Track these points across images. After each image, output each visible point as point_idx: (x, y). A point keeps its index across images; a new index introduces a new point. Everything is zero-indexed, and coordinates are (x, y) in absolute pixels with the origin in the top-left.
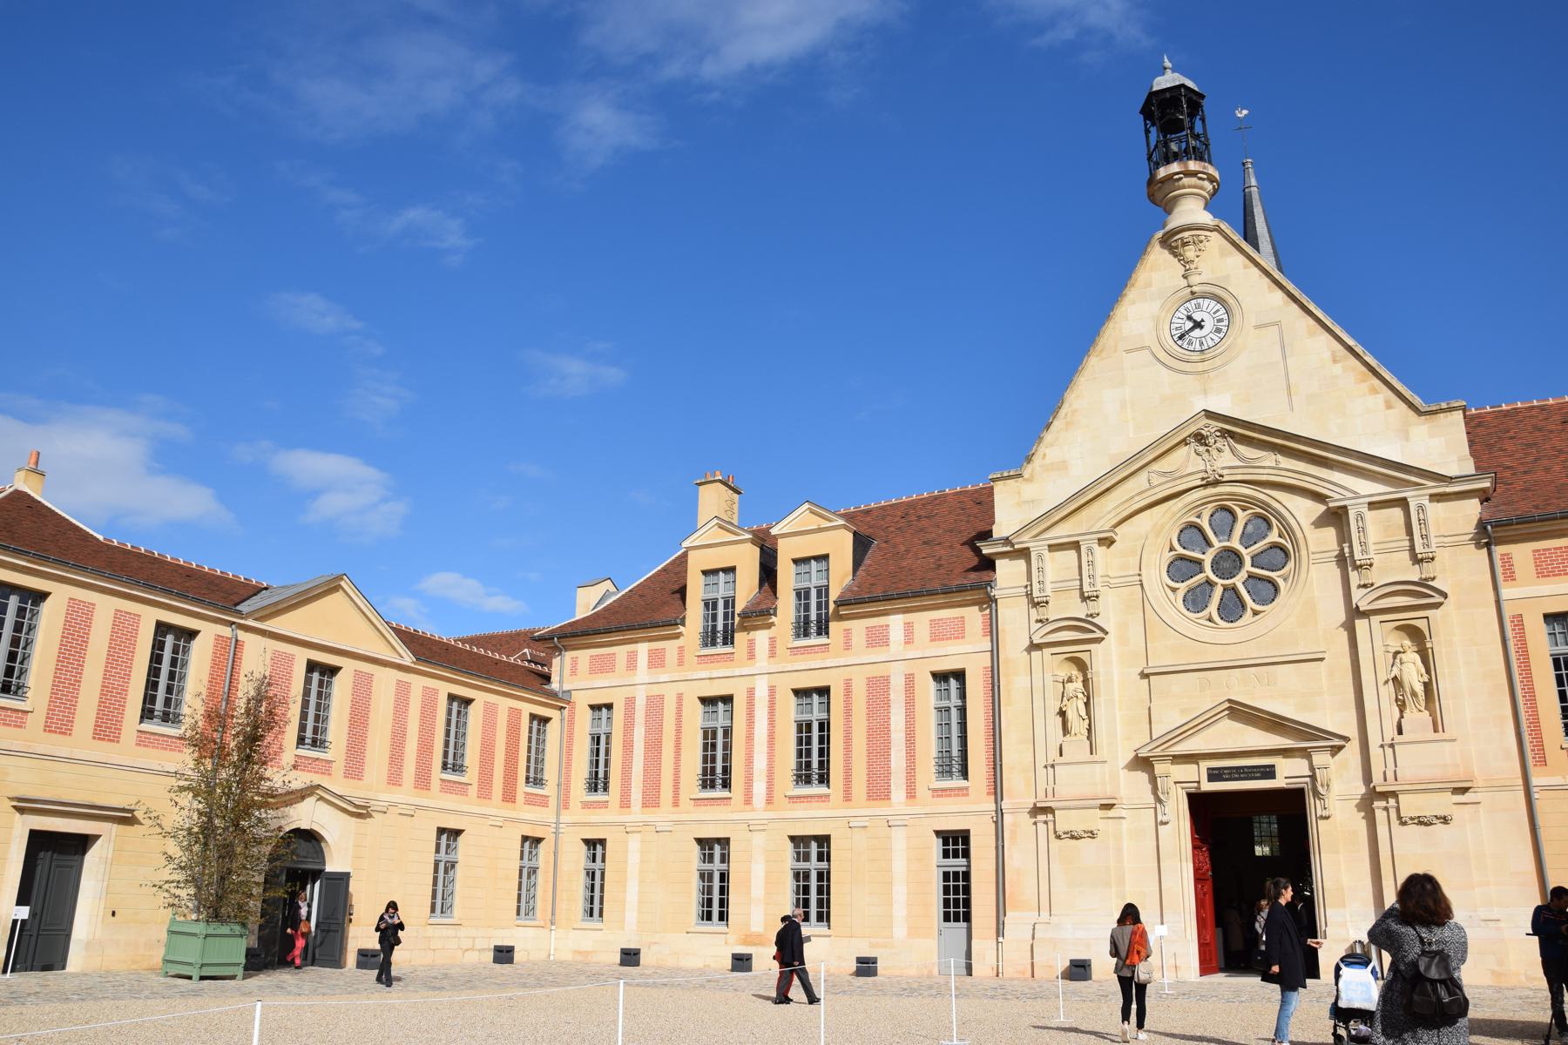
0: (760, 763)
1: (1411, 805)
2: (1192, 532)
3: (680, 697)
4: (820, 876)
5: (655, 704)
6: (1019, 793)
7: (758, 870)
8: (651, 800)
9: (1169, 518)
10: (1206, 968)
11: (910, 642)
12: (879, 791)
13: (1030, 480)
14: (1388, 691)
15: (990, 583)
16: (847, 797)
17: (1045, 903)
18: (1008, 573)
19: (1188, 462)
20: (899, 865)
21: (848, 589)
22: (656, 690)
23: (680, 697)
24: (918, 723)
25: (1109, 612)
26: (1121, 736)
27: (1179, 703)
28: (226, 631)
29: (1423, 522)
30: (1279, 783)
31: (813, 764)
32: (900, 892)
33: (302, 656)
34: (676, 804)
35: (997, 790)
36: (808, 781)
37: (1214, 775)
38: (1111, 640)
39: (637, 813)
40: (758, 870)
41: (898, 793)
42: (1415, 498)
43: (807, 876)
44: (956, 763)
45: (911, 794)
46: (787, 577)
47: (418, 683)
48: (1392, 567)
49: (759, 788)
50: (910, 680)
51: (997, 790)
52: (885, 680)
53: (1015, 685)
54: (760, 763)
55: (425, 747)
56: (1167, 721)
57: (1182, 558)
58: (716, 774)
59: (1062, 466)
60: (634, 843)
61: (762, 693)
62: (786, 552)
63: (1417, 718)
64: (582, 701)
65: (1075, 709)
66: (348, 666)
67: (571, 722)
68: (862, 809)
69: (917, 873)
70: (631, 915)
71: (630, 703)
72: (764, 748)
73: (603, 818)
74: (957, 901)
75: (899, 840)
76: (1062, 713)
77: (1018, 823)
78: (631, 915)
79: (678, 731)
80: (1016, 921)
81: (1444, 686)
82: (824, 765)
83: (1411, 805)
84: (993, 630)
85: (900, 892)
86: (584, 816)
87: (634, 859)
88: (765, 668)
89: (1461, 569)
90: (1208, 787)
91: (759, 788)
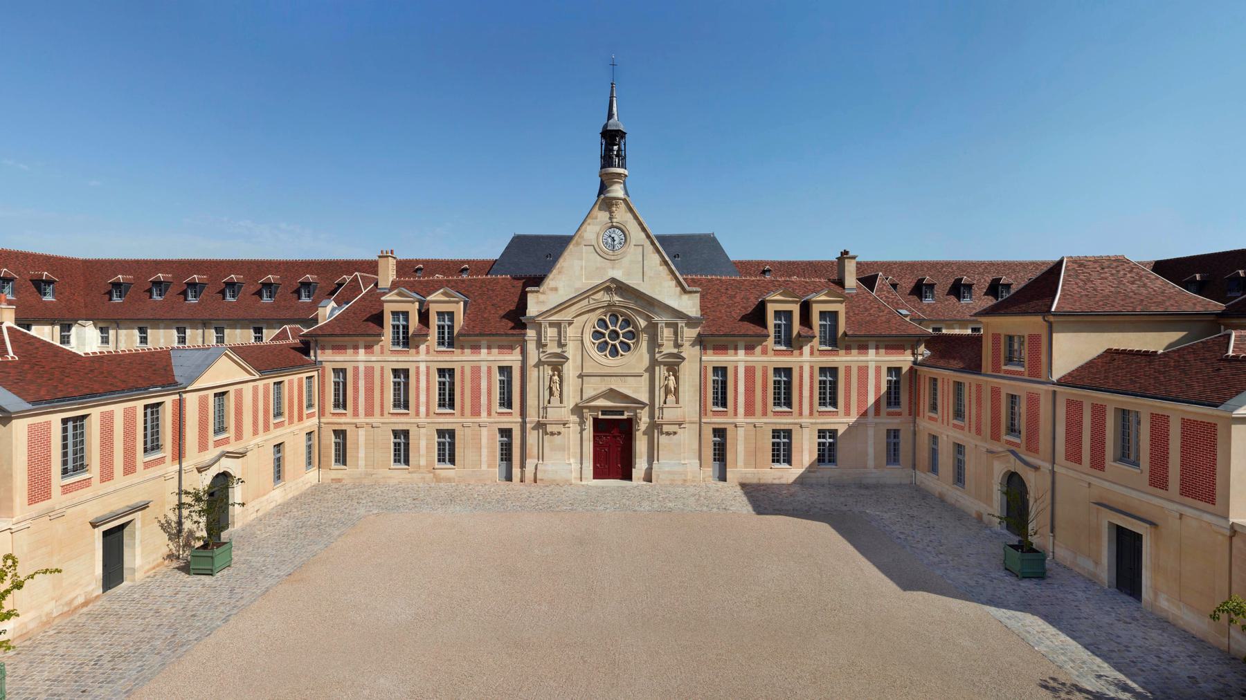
0: (423, 398)
1: (665, 428)
2: (602, 322)
3: (382, 368)
4: (404, 327)
5: (369, 372)
6: (532, 418)
7: (423, 443)
8: (369, 412)
9: (594, 318)
10: (598, 474)
11: (489, 358)
12: (476, 412)
13: (543, 293)
14: (663, 390)
15: (525, 335)
16: (462, 414)
17: (540, 456)
18: (531, 333)
19: (603, 297)
20: (484, 441)
21: (463, 328)
22: (369, 364)
23: (382, 368)
24: (490, 386)
25: (571, 351)
26: (571, 399)
27: (593, 387)
28: (177, 397)
29: (682, 332)
30: (625, 417)
31: (447, 399)
32: (484, 452)
33: (211, 393)
34: (382, 415)
35: (523, 413)
36: (444, 406)
37: (604, 413)
38: (570, 361)
39: (362, 419)
40: (423, 443)
41: (484, 414)
42: (681, 323)
43: (398, 327)
44: (507, 402)
45: (489, 414)
46: (434, 321)
47: (261, 384)
48: (668, 348)
49: (423, 409)
50: (489, 369)
51: (523, 413)
52: (479, 368)
53: (532, 374)
54: (423, 398)
55: (266, 412)
56: (588, 393)
57: (597, 332)
58: (402, 402)
59: (556, 289)
60: (362, 432)
61: (423, 367)
62: (434, 309)
63: (671, 398)
64: (329, 367)
65: (556, 387)
66: (232, 389)
67: (323, 376)
68: (469, 420)
69: (489, 443)
70: (362, 462)
71: (356, 369)
72: (424, 388)
73: (344, 420)
74: (506, 454)
75: (484, 431)
76: (551, 388)
77: (532, 437)
78: (362, 462)
79: (382, 383)
80: (530, 463)
81: (681, 389)
82: (452, 400)
83: (665, 428)
84: (524, 352)
85: (484, 452)
86: (335, 419)
87: (362, 439)
88: (424, 361)
89: (690, 353)
90: (600, 417)
91: (423, 409)
